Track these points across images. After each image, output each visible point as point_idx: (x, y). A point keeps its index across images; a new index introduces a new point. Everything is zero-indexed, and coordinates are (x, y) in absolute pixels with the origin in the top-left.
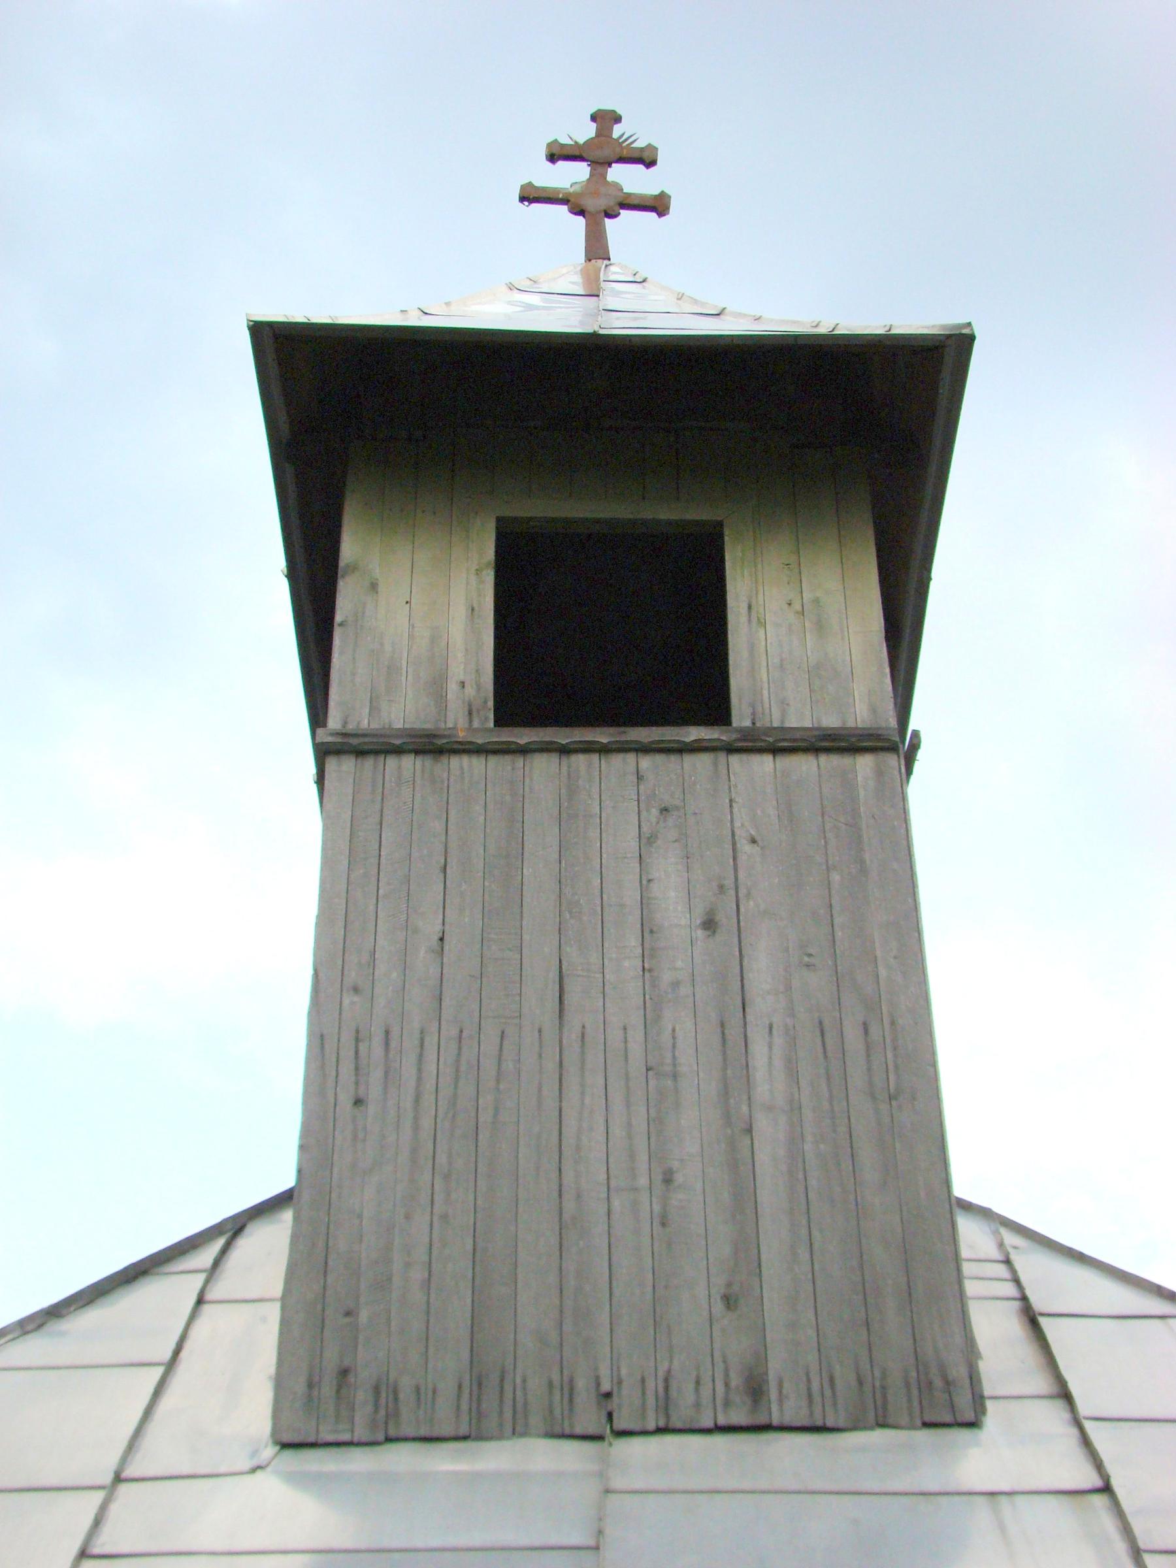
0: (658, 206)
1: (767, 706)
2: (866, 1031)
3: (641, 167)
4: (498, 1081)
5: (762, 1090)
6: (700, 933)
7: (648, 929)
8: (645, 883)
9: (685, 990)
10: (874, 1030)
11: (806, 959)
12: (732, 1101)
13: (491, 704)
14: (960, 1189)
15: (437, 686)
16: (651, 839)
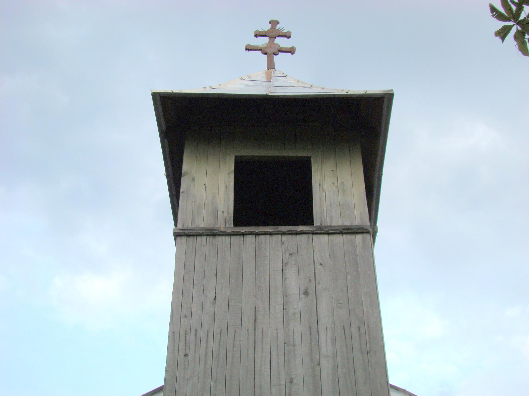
0: (291, 51)
1: (325, 218)
2: (359, 330)
3: (286, 38)
4: (233, 348)
5: (323, 350)
6: (303, 296)
7: (285, 295)
8: (284, 279)
9: (298, 316)
10: (362, 331)
11: (339, 305)
12: (313, 354)
13: (232, 219)
14: (391, 381)
15: (216, 217)
16: (287, 264)
